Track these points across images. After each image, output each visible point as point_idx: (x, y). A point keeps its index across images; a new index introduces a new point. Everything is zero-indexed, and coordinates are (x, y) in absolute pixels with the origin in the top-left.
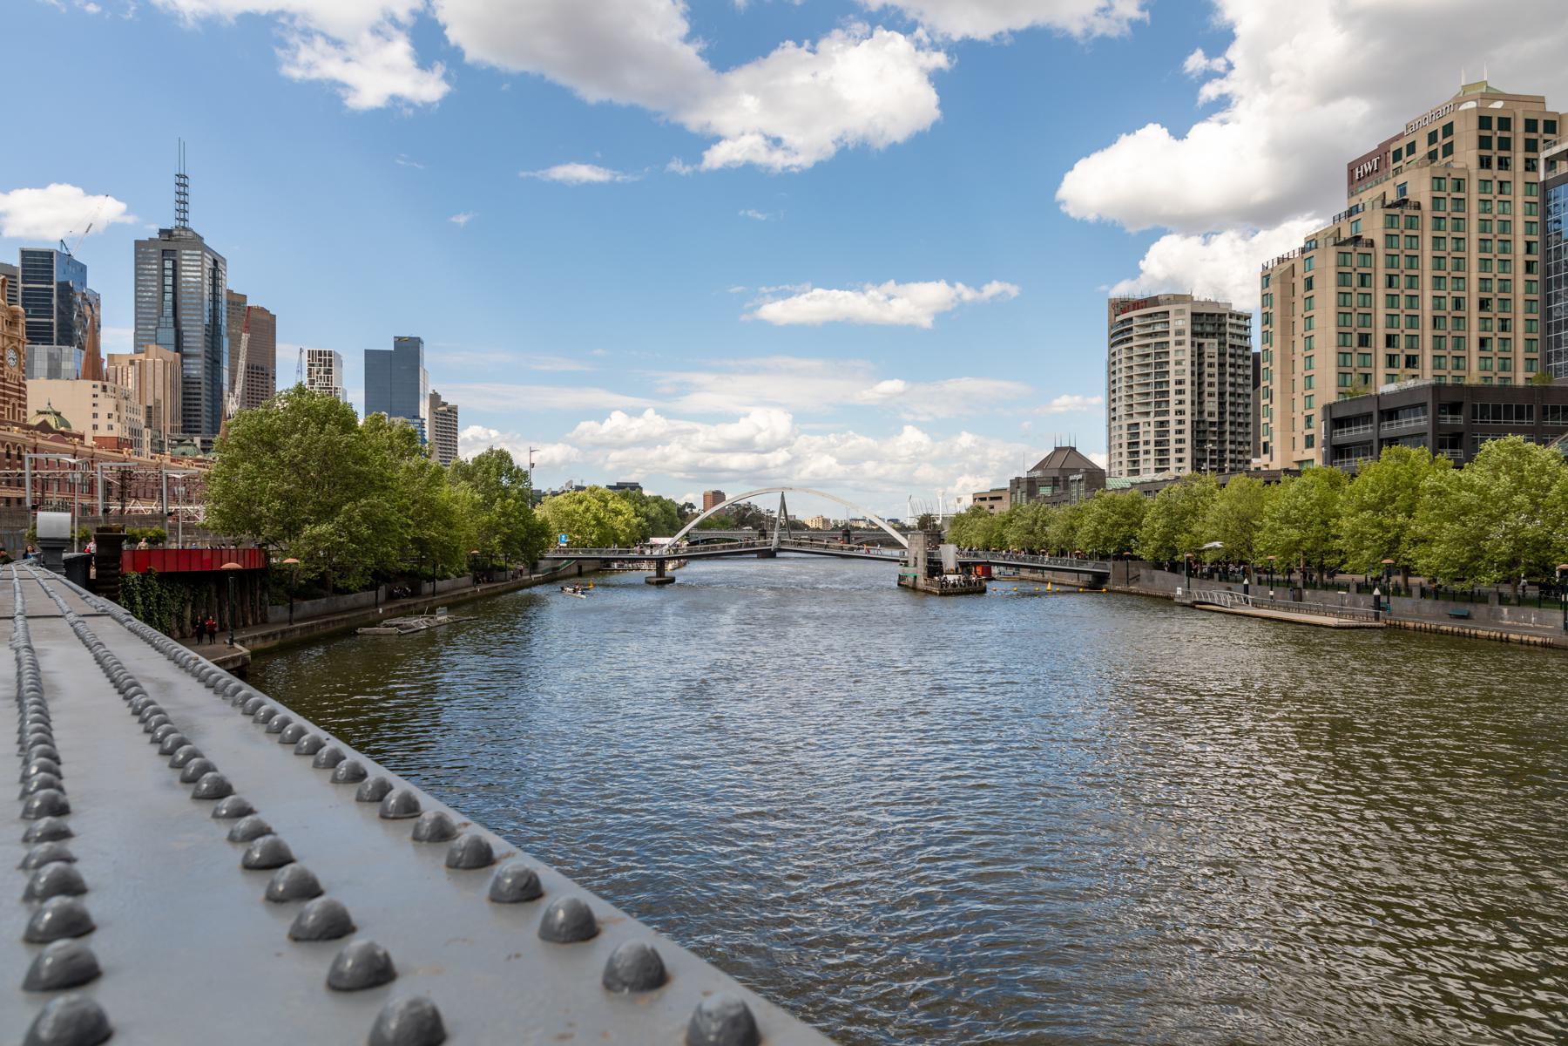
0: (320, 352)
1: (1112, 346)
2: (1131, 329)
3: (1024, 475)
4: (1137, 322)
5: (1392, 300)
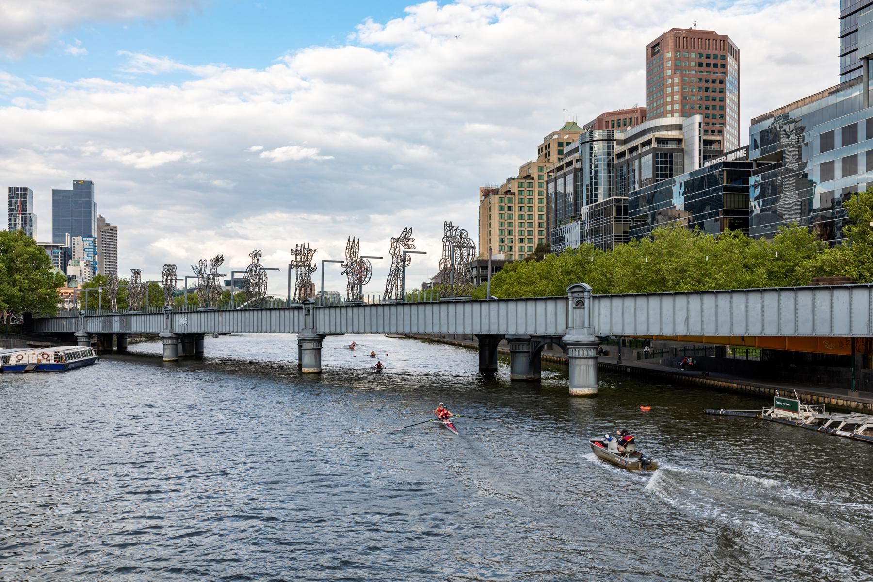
0: (18, 189)
5: (521, 217)
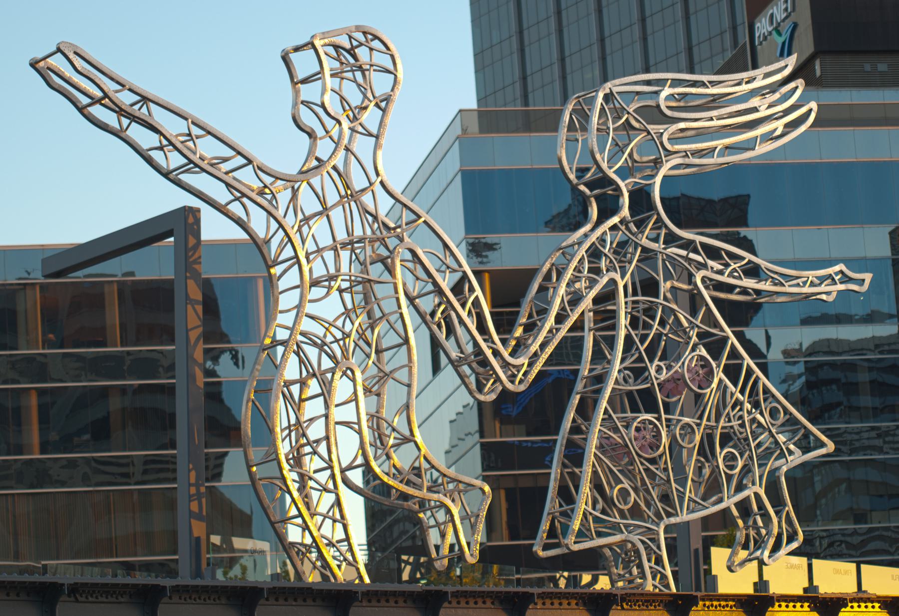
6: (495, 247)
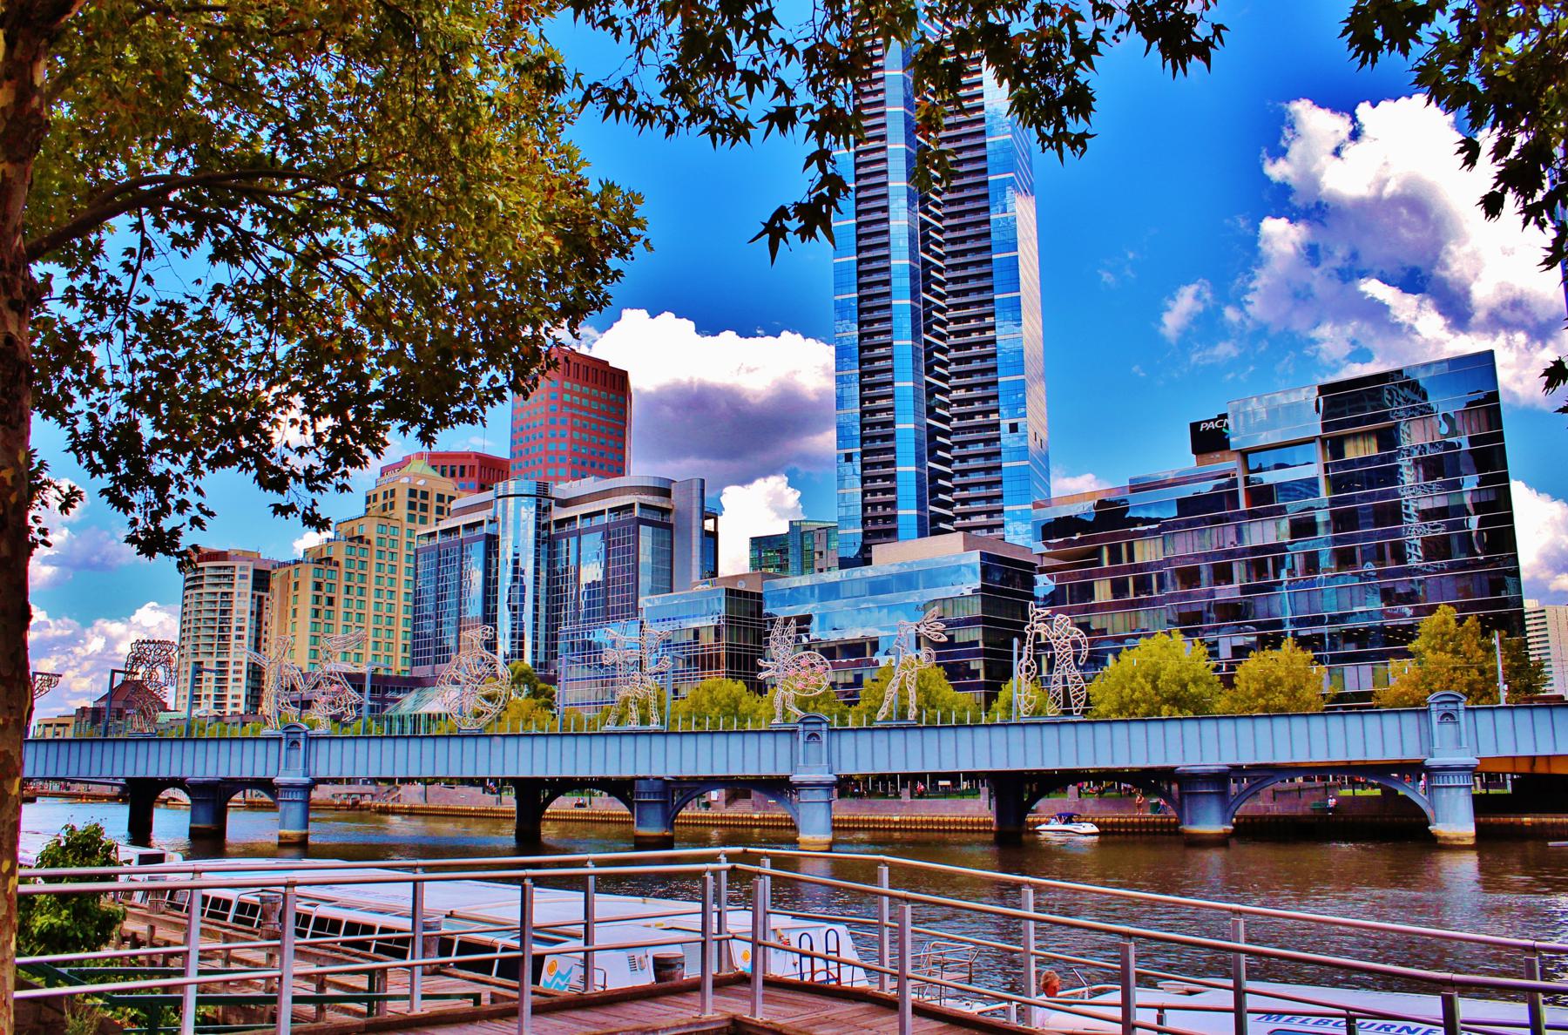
1: (188, 588)
2: (202, 577)
3: (91, 705)
4: (207, 572)
6: (1545, 266)
